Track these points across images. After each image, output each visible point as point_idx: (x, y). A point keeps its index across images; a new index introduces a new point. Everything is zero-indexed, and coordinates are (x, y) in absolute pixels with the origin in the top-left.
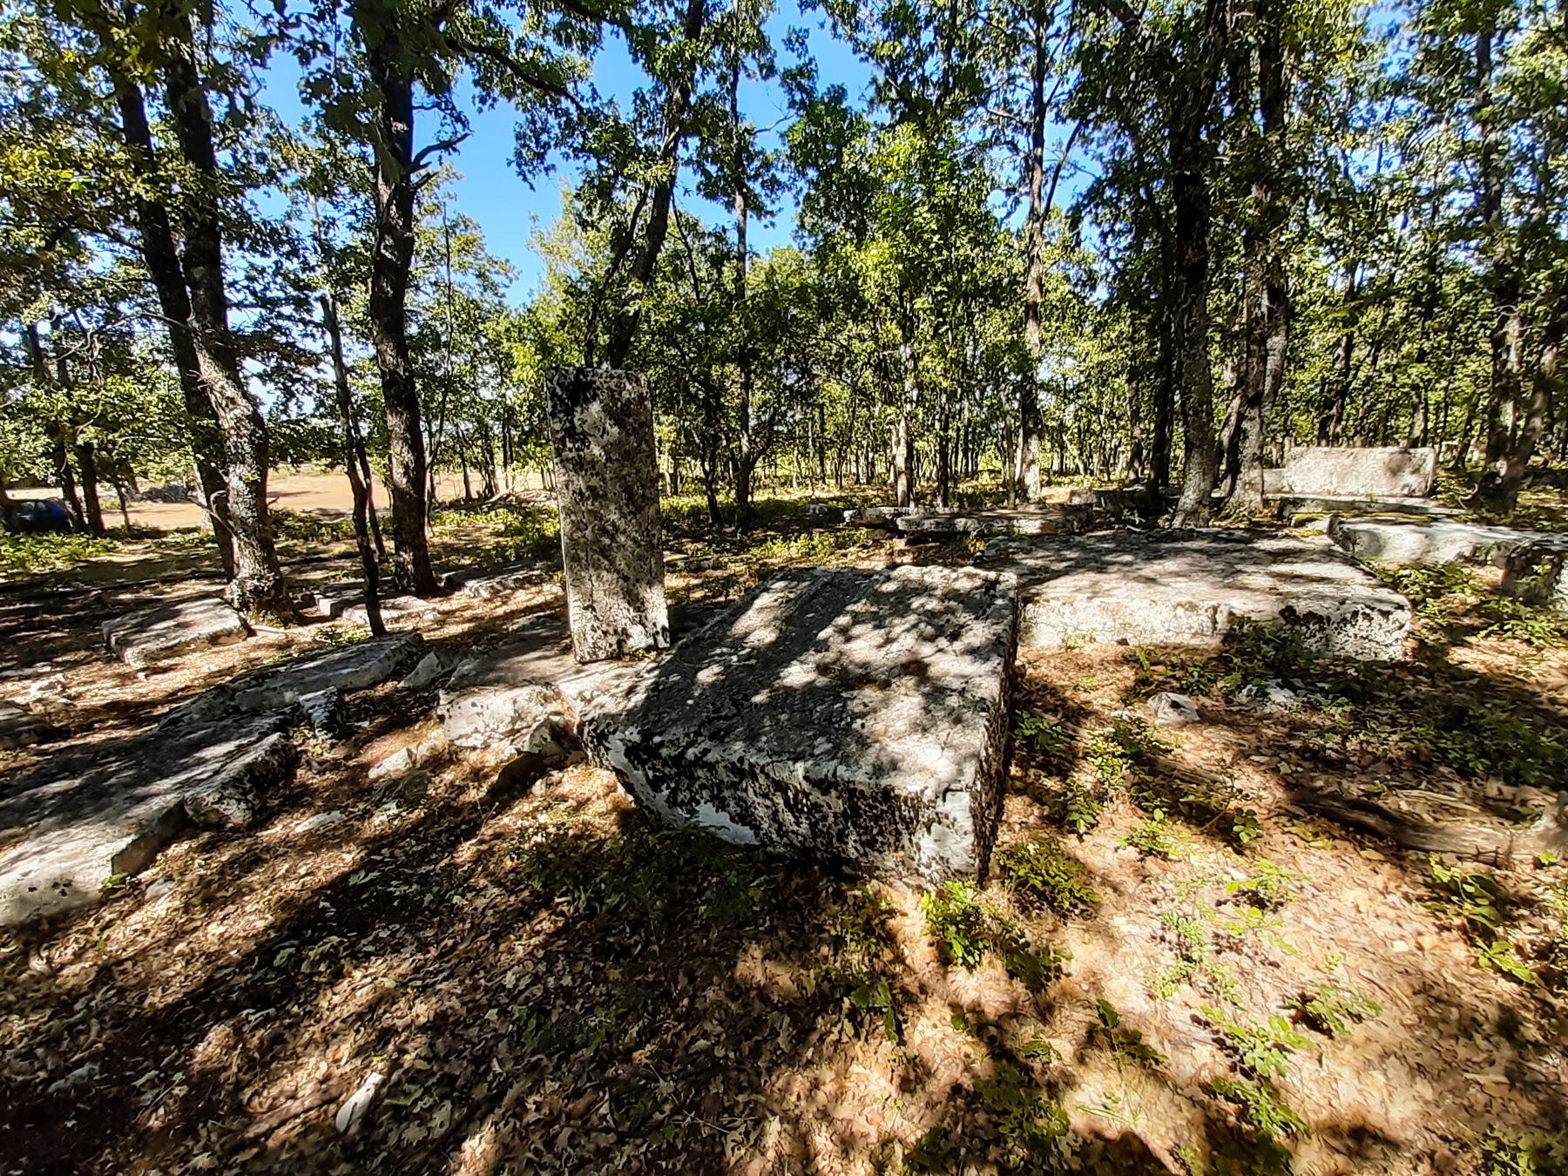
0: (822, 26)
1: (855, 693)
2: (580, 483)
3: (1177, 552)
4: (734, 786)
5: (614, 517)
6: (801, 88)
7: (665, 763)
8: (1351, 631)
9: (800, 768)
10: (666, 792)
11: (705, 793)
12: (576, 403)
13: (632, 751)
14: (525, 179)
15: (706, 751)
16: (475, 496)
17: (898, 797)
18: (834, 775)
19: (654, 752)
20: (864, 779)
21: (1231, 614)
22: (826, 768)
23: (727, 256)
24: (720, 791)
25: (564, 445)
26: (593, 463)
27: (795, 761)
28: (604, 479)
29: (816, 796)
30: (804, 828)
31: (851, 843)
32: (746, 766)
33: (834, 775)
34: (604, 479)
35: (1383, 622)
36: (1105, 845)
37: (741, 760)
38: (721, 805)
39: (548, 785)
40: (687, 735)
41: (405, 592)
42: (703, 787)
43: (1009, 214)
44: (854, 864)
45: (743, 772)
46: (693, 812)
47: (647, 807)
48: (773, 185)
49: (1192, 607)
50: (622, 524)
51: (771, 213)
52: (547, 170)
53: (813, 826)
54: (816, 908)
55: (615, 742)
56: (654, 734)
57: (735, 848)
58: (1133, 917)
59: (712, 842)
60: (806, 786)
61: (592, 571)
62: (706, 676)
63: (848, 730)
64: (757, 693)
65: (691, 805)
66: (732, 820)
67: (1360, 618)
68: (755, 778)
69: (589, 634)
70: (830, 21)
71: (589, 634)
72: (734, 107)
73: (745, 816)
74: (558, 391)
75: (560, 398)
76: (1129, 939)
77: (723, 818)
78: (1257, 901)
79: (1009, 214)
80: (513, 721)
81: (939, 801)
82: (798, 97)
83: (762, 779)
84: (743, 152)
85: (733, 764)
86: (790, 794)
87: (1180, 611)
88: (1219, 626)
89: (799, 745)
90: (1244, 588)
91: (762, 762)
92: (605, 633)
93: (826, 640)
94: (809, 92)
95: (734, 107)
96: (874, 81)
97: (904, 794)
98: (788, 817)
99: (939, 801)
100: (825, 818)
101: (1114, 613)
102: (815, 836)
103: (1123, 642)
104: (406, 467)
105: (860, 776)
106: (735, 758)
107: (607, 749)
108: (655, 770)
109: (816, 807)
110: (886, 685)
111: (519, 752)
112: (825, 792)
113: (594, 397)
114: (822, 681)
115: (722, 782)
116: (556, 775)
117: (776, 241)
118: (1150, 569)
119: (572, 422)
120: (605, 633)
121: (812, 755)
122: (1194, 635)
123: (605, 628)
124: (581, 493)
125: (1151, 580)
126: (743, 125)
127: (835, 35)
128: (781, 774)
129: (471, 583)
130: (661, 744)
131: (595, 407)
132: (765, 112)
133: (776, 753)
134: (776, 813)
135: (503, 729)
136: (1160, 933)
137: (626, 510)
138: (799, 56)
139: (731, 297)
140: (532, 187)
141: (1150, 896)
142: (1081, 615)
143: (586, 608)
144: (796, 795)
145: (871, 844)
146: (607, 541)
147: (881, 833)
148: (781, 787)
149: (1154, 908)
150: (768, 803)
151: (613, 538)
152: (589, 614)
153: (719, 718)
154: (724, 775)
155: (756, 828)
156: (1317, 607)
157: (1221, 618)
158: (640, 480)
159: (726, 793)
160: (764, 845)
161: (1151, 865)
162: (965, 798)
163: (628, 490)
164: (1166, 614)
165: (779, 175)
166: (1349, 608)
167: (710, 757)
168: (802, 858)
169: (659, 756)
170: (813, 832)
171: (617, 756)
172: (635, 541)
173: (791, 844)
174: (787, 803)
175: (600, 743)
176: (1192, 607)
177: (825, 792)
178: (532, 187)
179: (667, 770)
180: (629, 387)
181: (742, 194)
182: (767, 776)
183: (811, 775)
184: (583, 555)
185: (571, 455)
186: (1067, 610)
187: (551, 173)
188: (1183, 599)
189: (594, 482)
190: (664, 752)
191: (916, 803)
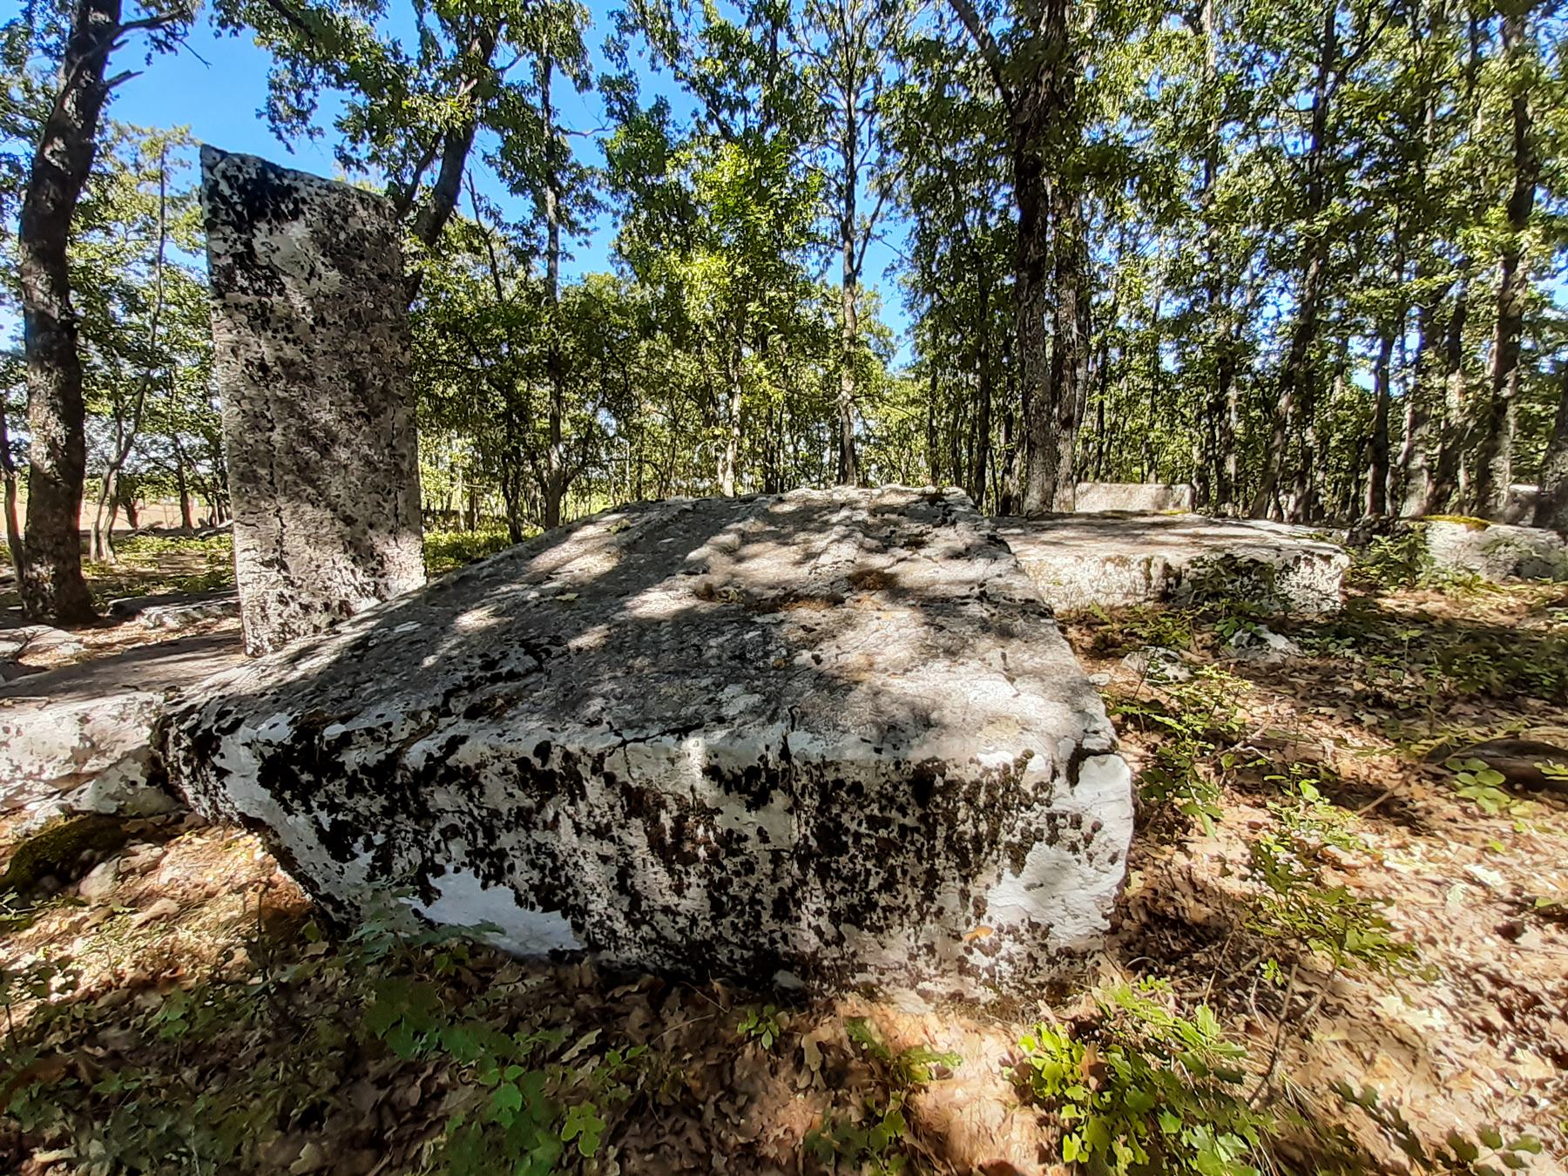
0: (640, 53)
1: (780, 616)
2: (264, 349)
3: (1065, 526)
4: (524, 818)
5: (326, 417)
6: (621, 100)
7: (354, 787)
9: (695, 749)
10: (365, 858)
11: (457, 848)
12: (257, 214)
13: (276, 771)
14: (280, 137)
15: (454, 744)
16: (196, 525)
17: (951, 786)
18: (785, 754)
19: (326, 764)
20: (862, 753)
21: (1167, 567)
22: (763, 740)
23: (534, 251)
24: (491, 836)
25: (231, 279)
26: (289, 323)
27: (683, 731)
28: (309, 352)
29: (735, 815)
30: (694, 899)
31: (807, 917)
32: (555, 764)
33: (785, 754)
34: (309, 352)
35: (1325, 567)
37: (543, 750)
38: (493, 868)
39: (121, 876)
40: (415, 716)
41: (38, 620)
42: (451, 832)
43: (822, 272)
44: (808, 966)
45: (546, 779)
46: (429, 895)
47: (328, 898)
48: (589, 202)
50: (344, 432)
51: (586, 231)
52: (310, 133)
53: (716, 889)
54: (731, 1093)
55: (238, 754)
56: (327, 722)
57: (524, 963)
59: (473, 964)
60: (709, 792)
61: (281, 500)
62: (473, 619)
63: (788, 669)
64: (579, 632)
65: (423, 882)
66: (520, 901)
67: (1302, 564)
68: (576, 790)
69: (273, 608)
70: (648, 51)
71: (273, 608)
72: (545, 100)
73: (553, 891)
74: (224, 187)
75: (224, 200)
77: (498, 903)
79: (822, 272)
80: (78, 757)
81: (1061, 784)
82: (617, 108)
83: (594, 787)
84: (556, 152)
85: (523, 763)
86: (666, 820)
87: (1110, 567)
88: (1154, 583)
89: (685, 702)
91: (596, 747)
92: (306, 608)
93: (702, 561)
94: (632, 107)
95: (545, 100)
96: (695, 114)
97: (970, 774)
98: (654, 878)
100: (749, 867)
102: (718, 910)
104: (53, 444)
105: (851, 749)
106: (527, 749)
107: (222, 773)
108: (333, 808)
109: (731, 842)
110: (835, 601)
111: (69, 812)
112: (758, 801)
113: (296, 214)
114: (705, 607)
115: (495, 813)
116: (145, 853)
117: (592, 260)
118: (1049, 536)
119: (248, 245)
120: (306, 608)
121: (721, 720)
122: (1126, 595)
123: (305, 598)
124: (263, 367)
125: (1045, 543)
126: (554, 123)
127: (653, 68)
128: (642, 769)
129: (154, 611)
130: (345, 740)
131: (297, 231)
132: (584, 127)
133: (629, 725)
134: (625, 873)
135: (51, 773)
137: (349, 409)
138: (618, 66)
139: (539, 296)
140: (289, 148)
143: (268, 564)
144: (679, 821)
145: (855, 916)
146: (314, 455)
147: (888, 885)
148: (639, 802)
150: (609, 849)
151: (325, 451)
152: (273, 574)
153: (496, 678)
154: (500, 795)
155: (576, 913)
157: (1156, 572)
158: (381, 364)
159: (506, 840)
160: (595, 947)
163: (356, 376)
164: (1095, 571)
165: (595, 193)
167: (465, 756)
168: (685, 970)
169: (338, 770)
170: (716, 906)
171: (244, 792)
172: (368, 462)
173: (660, 940)
174: (656, 844)
175: (204, 760)
176: (1123, 562)
177: (758, 801)
178: (289, 148)
179: (362, 803)
180: (361, 212)
181: (553, 189)
182: (610, 780)
183: (726, 764)
184: (262, 472)
185: (244, 299)
187: (317, 138)
188: (1113, 554)
189: (290, 352)
190: (352, 759)
191: (1003, 794)
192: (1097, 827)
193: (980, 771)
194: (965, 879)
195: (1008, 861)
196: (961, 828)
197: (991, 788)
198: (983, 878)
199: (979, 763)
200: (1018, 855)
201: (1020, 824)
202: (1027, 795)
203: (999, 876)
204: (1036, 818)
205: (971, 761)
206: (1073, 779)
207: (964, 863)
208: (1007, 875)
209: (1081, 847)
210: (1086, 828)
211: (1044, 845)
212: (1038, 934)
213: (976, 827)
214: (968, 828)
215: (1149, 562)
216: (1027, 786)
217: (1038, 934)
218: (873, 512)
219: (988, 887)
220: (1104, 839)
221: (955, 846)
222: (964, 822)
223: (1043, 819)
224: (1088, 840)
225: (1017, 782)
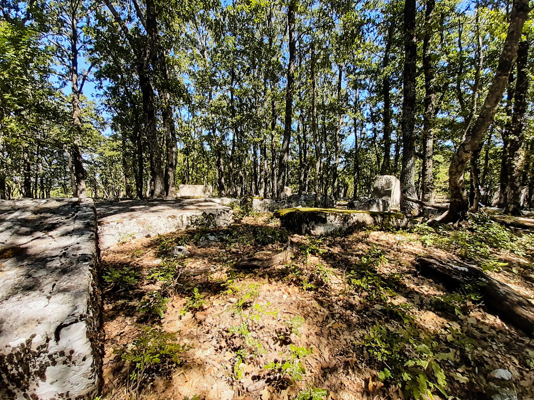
8: (221, 218)
36: (175, 316)
49: (174, 217)
58: (203, 347)
76: (208, 361)
78: (245, 306)
87: (170, 219)
90: (188, 209)
99: (52, 343)
101: (143, 224)
103: (148, 236)
125: (153, 212)
136: (218, 346)
141: (205, 331)
142: (128, 227)
149: (210, 336)
156: (211, 212)
161: (200, 316)
162: (82, 326)
164: (165, 221)
166: (219, 211)
176: (174, 217)
186: (119, 225)
188: (171, 215)
192: (72, 352)
193: (11, 349)
194: (24, 390)
195: (38, 378)
196: (12, 372)
197: (18, 354)
198: (31, 387)
199: (10, 346)
200: (41, 374)
201: (37, 363)
202: (35, 352)
203: (37, 385)
204: (44, 358)
205: (6, 346)
206: (57, 339)
207: (19, 386)
208: (40, 382)
209: (68, 361)
210: (67, 354)
211: (51, 367)
212: (65, 397)
213: (18, 370)
214: (14, 371)
215: (182, 216)
216: (34, 348)
217: (65, 397)
218: (35, 213)
219: (35, 390)
220: (77, 355)
221: (12, 379)
222: (12, 370)
223: (47, 358)
224: (70, 358)
225: (29, 350)
